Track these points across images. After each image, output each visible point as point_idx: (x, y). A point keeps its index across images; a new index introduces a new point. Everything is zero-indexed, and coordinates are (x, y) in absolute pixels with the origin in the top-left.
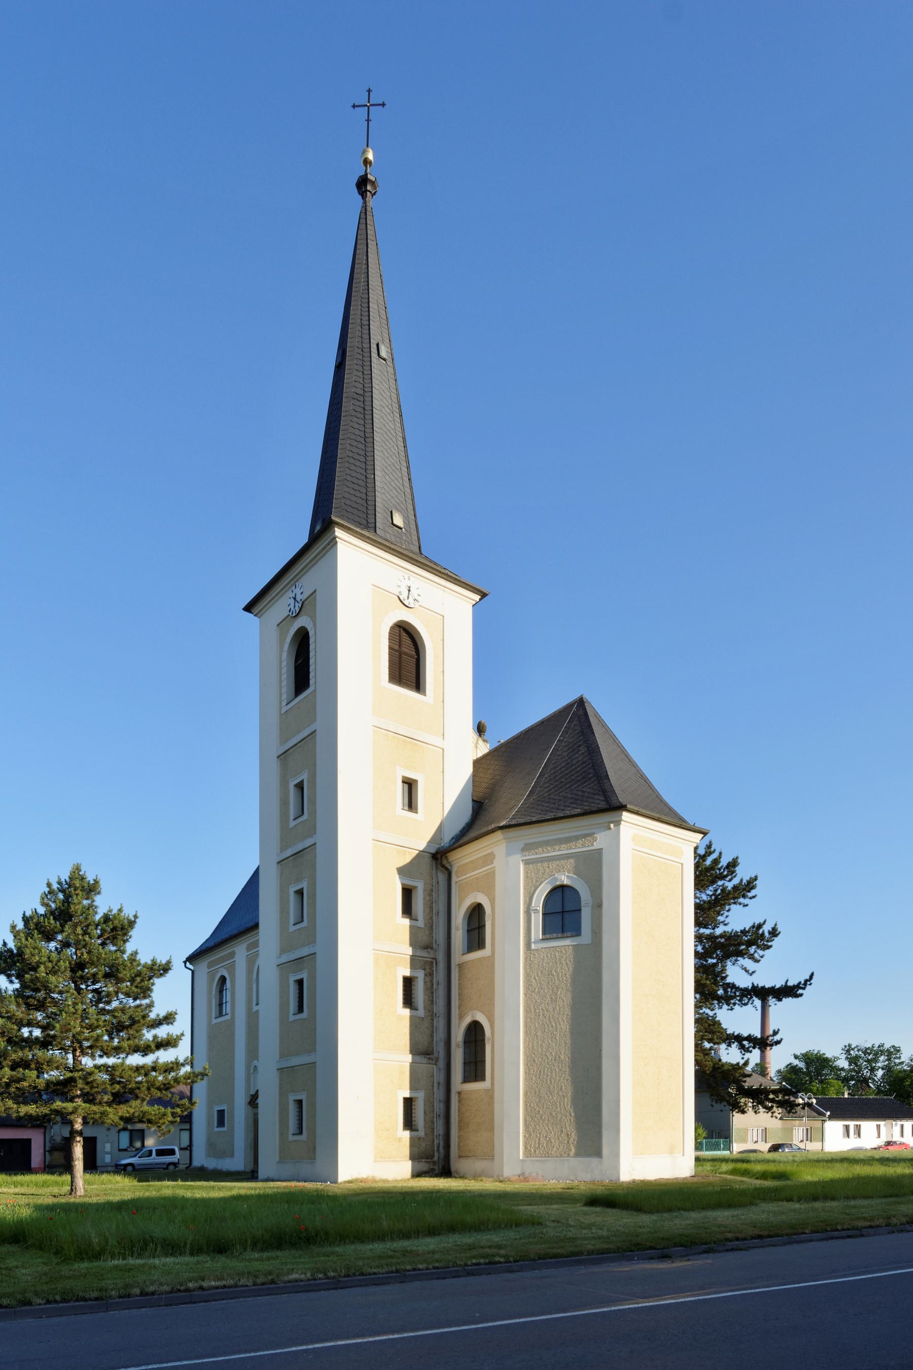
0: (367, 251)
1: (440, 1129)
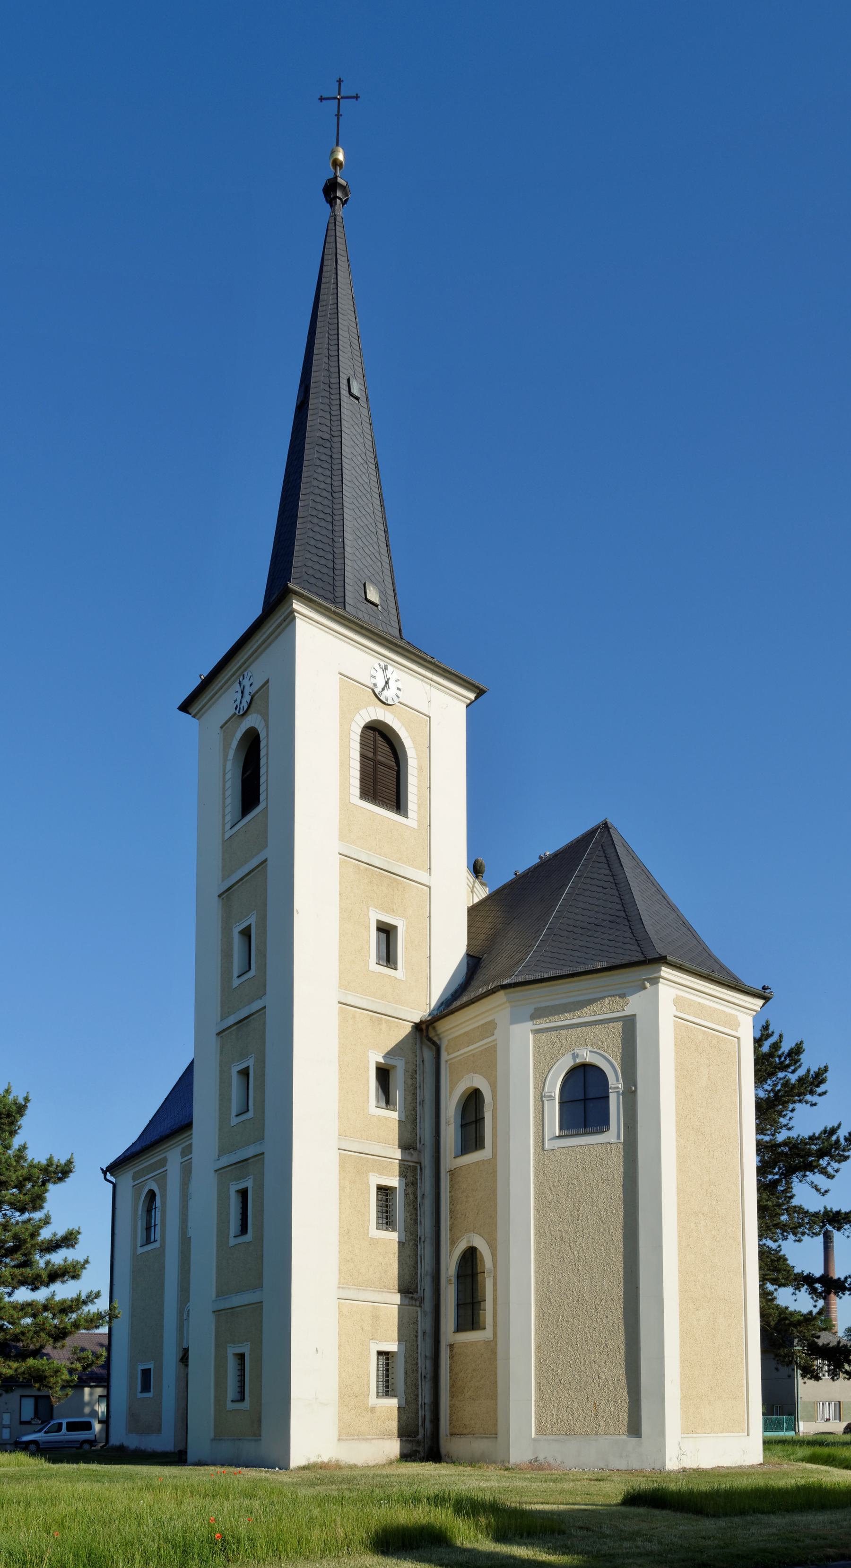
0: (336, 268)
1: (426, 1397)
